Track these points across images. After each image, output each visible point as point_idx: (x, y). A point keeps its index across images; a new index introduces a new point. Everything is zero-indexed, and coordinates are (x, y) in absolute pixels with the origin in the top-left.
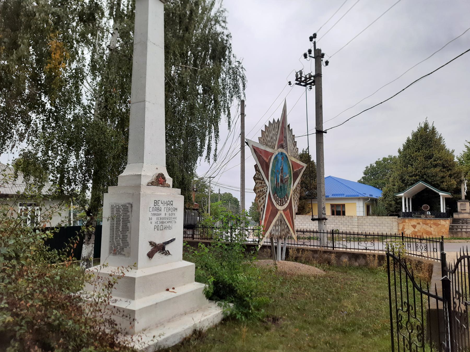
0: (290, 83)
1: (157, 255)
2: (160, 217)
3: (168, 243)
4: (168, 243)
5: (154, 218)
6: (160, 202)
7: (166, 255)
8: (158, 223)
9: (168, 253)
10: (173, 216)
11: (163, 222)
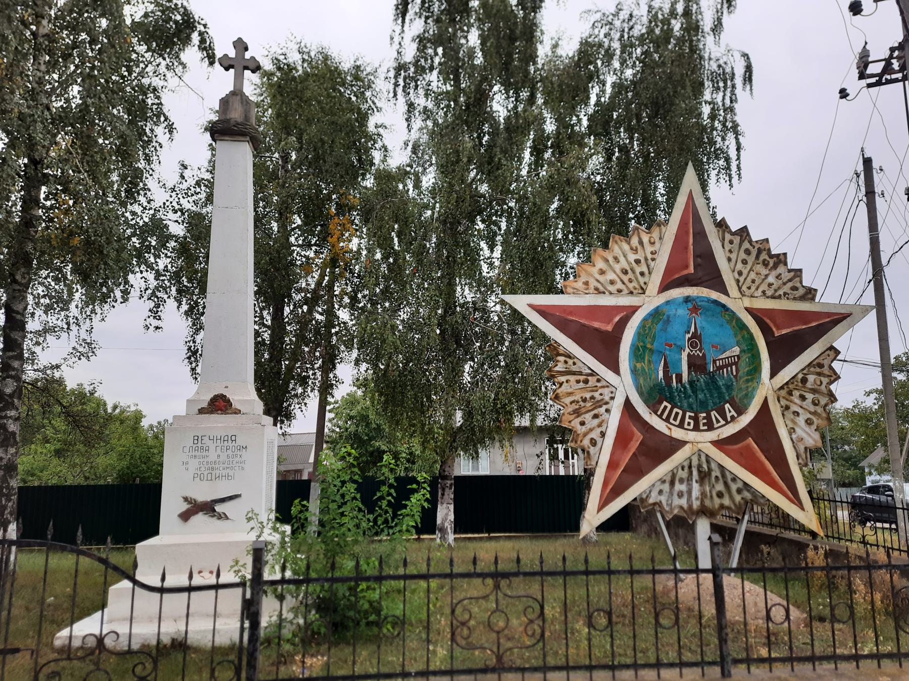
0: (843, 94)
1: (200, 519)
2: (205, 460)
3: (223, 500)
4: (223, 500)
5: (194, 464)
6: (206, 439)
7: (219, 519)
8: (203, 469)
9: (223, 517)
10: (238, 459)
11: (213, 469)
